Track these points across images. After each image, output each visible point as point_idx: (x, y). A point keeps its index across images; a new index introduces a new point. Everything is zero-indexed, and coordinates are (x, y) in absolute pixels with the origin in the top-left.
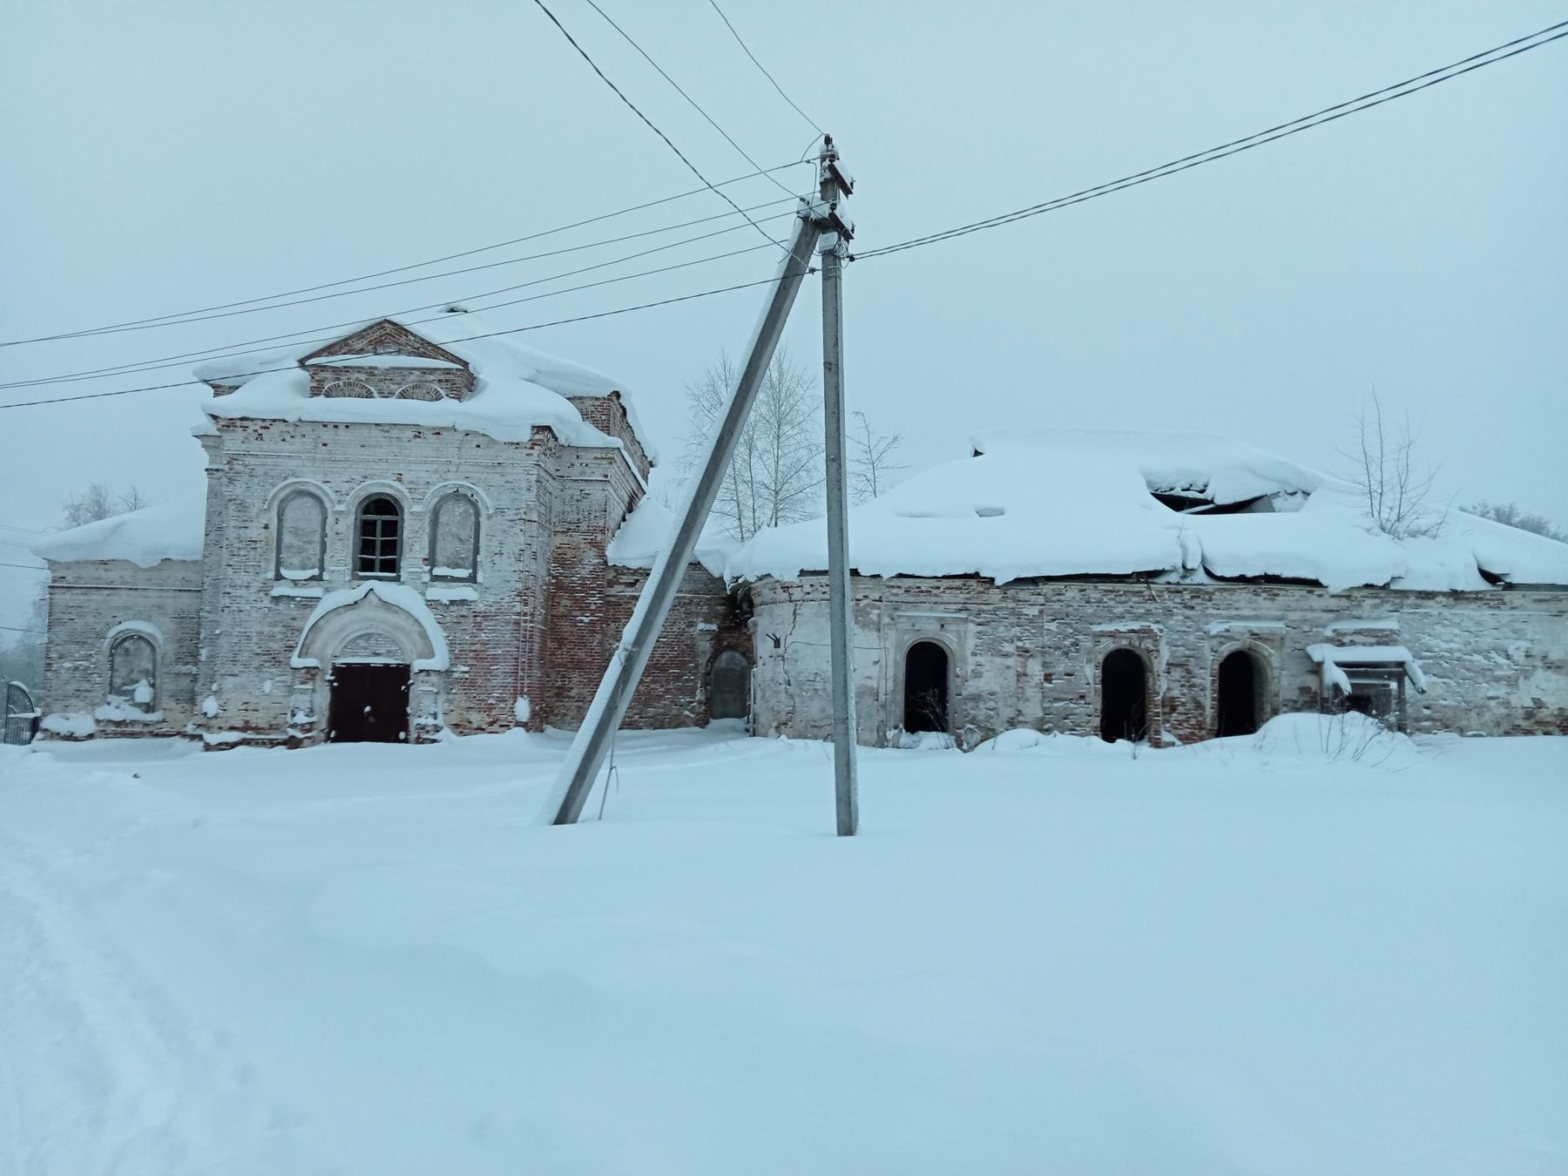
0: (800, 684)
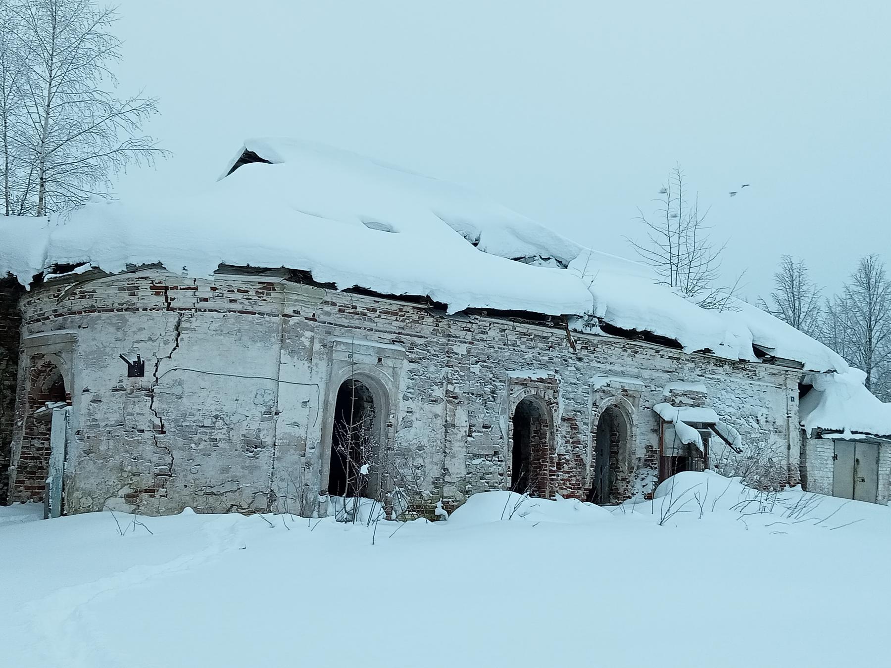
0: (183, 432)
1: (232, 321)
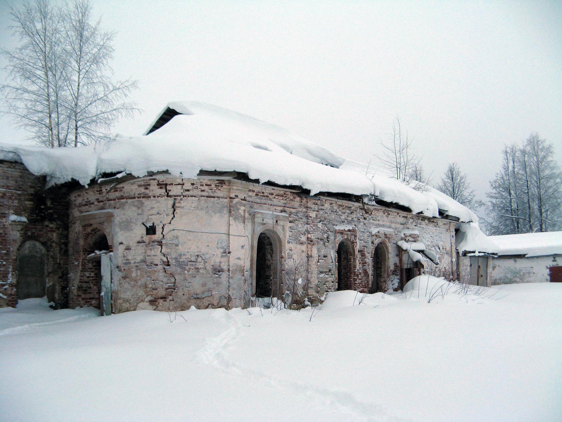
0: (181, 265)
1: (203, 202)
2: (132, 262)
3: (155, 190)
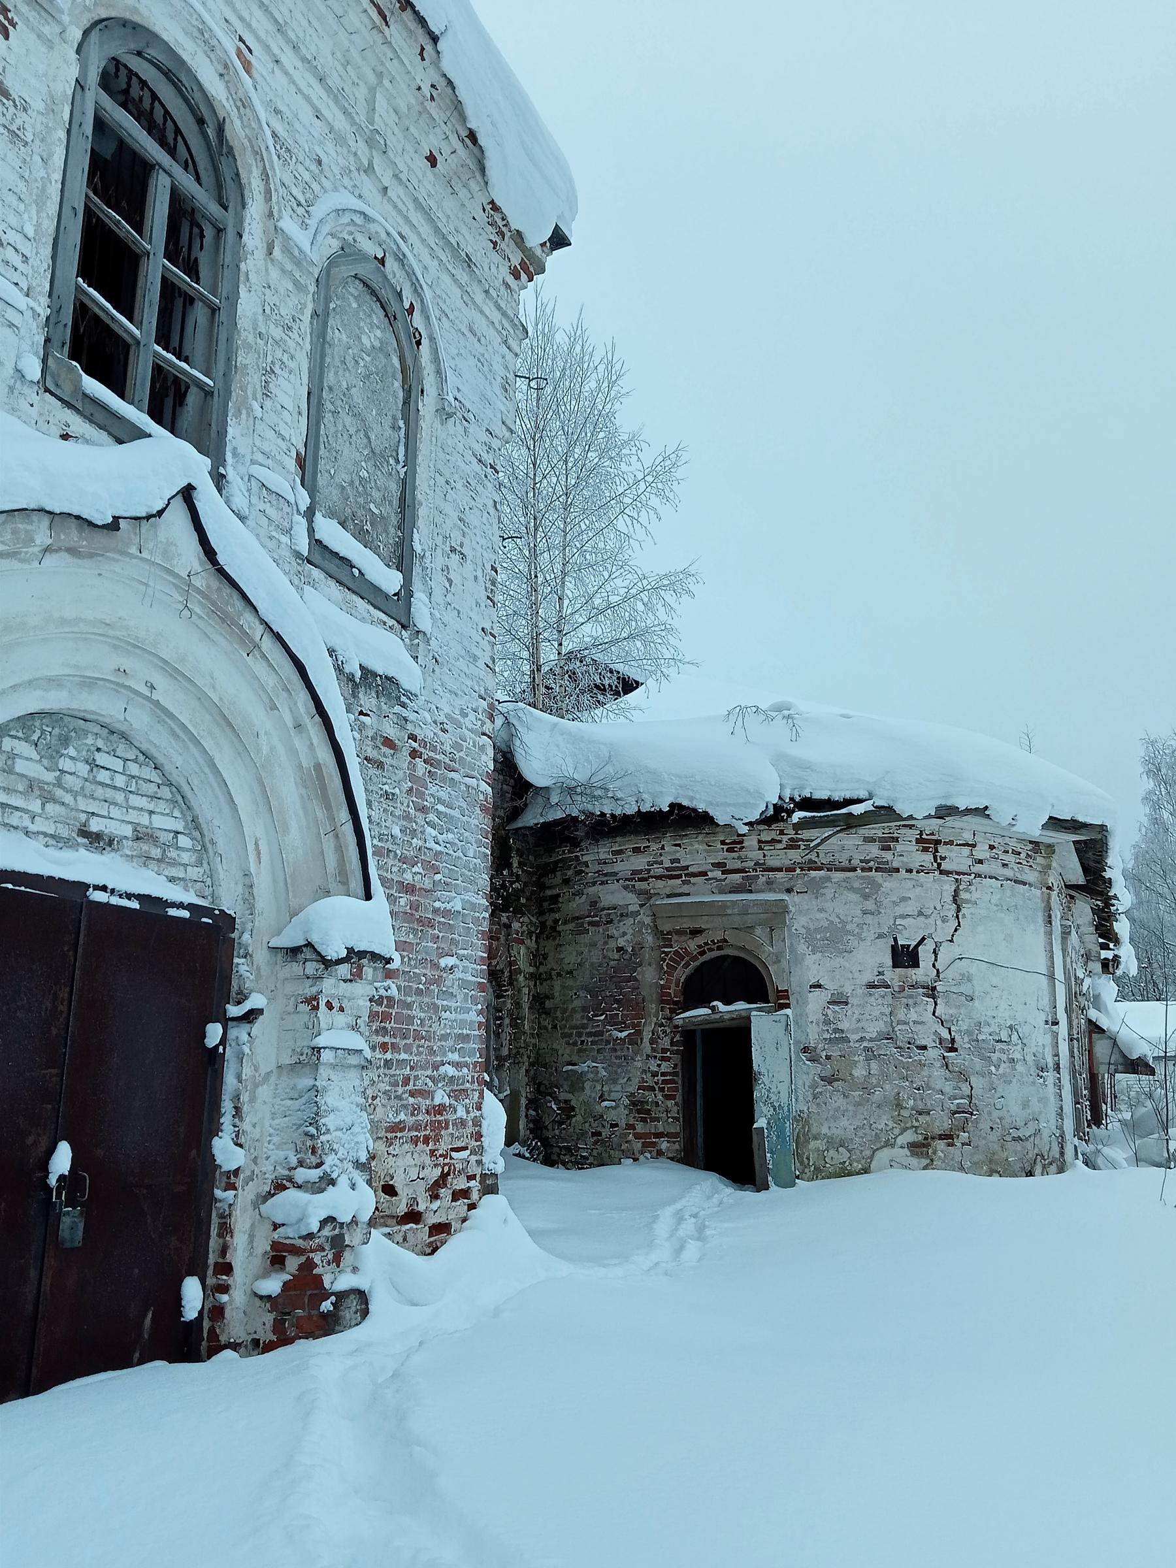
2: (854, 1037)
3: (909, 853)
